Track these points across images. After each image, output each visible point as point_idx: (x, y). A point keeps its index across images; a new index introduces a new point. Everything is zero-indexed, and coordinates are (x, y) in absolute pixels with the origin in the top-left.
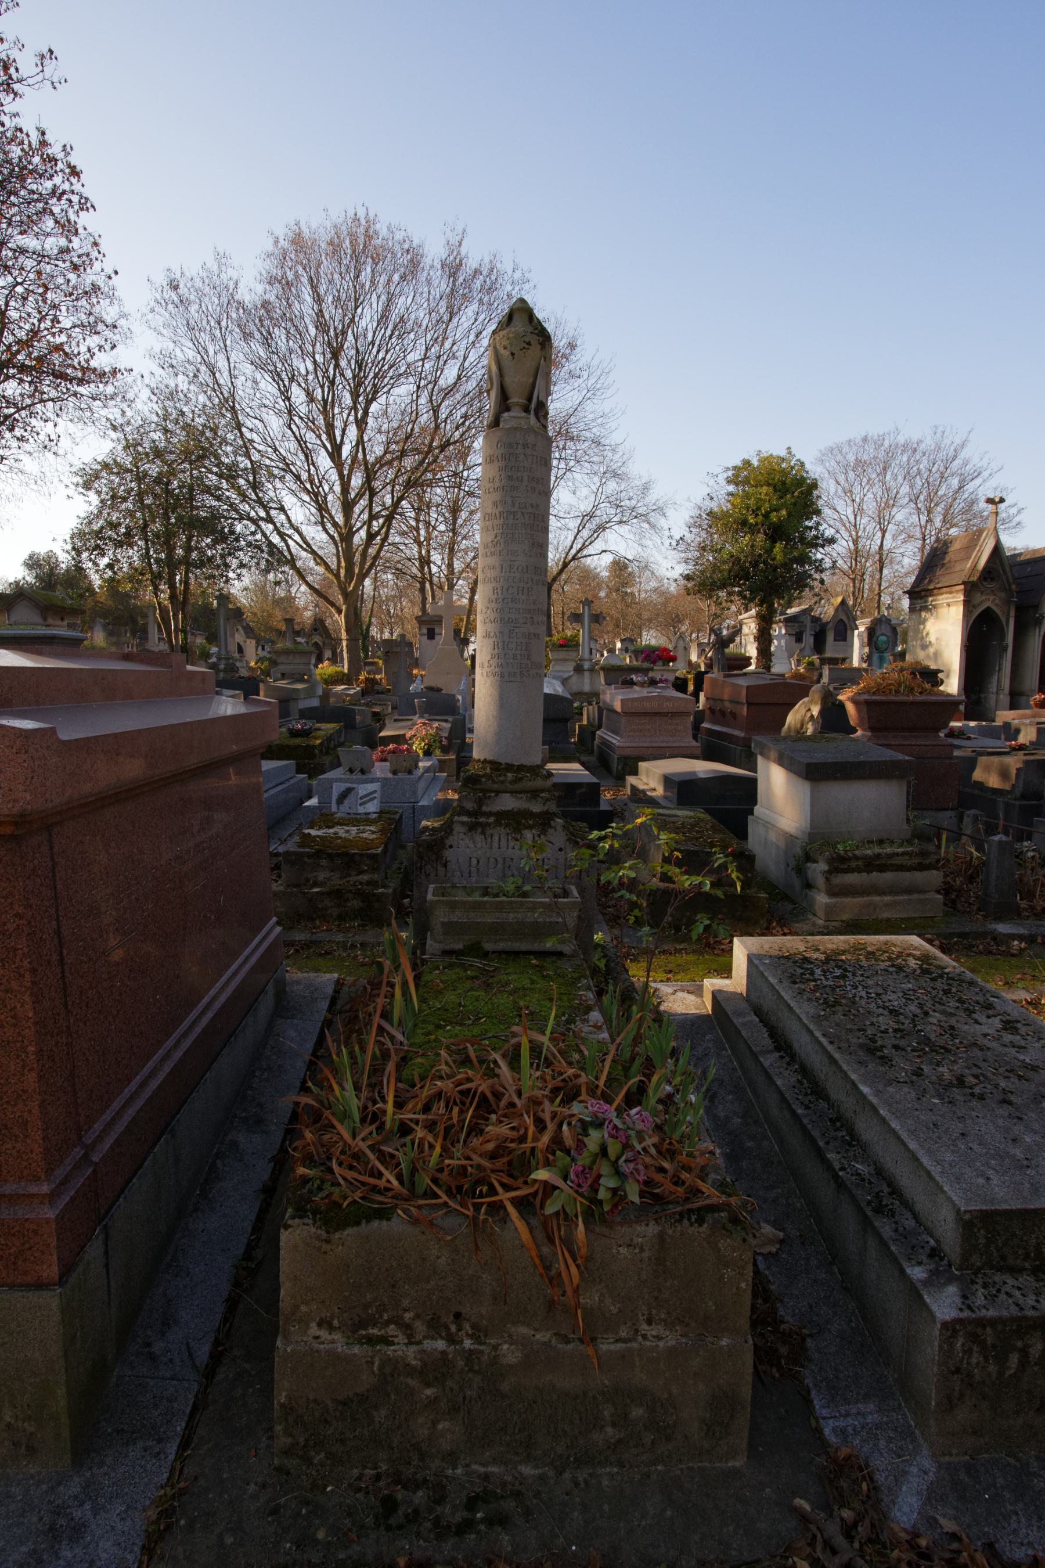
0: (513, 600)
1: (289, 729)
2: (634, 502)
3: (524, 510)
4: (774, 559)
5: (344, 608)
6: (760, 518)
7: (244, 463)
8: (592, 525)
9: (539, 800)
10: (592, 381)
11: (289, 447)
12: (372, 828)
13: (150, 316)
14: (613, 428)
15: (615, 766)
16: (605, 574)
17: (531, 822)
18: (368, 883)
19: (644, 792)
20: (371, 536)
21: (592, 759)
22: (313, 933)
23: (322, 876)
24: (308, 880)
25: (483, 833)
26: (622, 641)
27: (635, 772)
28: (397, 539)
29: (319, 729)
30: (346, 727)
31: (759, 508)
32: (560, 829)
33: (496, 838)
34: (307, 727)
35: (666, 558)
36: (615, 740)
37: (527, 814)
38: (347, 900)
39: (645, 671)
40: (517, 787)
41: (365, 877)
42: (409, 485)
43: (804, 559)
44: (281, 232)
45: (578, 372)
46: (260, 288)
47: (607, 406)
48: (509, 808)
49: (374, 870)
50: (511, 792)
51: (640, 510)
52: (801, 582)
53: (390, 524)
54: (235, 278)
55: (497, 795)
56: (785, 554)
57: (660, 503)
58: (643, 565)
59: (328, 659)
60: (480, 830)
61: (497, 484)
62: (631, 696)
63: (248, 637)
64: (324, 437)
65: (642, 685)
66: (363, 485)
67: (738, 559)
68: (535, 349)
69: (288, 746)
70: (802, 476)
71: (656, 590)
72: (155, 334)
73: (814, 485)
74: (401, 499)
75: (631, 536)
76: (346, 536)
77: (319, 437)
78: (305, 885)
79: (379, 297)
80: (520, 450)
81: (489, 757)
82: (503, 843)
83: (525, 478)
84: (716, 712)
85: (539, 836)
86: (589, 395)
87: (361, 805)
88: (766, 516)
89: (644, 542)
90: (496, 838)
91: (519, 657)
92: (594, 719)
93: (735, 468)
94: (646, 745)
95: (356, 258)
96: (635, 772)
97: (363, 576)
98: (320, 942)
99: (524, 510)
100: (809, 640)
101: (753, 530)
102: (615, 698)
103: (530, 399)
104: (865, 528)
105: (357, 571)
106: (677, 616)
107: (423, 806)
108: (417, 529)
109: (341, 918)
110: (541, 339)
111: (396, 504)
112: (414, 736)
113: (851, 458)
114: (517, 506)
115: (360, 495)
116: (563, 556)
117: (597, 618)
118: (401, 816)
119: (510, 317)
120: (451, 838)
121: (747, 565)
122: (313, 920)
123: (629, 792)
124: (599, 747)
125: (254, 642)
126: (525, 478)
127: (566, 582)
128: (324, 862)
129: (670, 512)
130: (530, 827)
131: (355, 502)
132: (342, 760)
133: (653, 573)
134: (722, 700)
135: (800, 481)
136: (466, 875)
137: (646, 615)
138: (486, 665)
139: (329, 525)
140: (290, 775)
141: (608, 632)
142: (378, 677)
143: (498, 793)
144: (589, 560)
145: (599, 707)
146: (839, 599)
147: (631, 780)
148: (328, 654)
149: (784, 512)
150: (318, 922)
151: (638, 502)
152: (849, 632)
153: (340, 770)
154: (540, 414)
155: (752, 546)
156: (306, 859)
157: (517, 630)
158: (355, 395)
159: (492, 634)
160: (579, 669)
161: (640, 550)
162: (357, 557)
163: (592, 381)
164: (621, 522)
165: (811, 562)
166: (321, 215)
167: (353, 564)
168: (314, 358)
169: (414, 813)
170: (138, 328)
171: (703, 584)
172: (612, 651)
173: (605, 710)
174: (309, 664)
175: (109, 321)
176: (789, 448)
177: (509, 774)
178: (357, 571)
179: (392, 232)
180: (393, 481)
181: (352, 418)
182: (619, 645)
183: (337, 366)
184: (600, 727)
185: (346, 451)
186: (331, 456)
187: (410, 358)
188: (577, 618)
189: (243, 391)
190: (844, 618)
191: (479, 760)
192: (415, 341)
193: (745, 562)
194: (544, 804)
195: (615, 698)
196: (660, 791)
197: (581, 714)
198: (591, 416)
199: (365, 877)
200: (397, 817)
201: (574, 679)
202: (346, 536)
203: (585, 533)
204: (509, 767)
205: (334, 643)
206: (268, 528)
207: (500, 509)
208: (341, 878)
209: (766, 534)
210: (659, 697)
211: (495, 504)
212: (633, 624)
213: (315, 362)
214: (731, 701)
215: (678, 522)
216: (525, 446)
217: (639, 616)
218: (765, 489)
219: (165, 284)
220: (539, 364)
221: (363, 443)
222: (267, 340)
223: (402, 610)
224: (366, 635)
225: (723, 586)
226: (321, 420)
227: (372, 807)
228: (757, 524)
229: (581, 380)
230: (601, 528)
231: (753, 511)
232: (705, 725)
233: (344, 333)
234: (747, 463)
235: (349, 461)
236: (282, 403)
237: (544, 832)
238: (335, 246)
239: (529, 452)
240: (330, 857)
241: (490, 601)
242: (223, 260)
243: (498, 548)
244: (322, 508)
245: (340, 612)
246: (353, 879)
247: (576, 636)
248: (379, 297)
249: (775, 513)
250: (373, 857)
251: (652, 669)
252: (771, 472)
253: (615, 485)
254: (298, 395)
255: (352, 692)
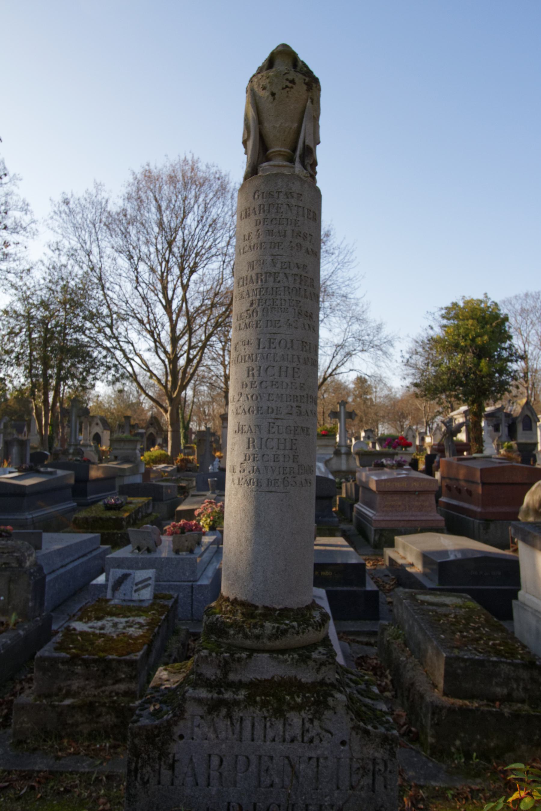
0: (273, 384)
1: (105, 504)
2: (371, 337)
3: (287, 271)
4: (481, 371)
5: (169, 409)
6: (469, 342)
7: (105, 311)
8: (342, 352)
9: (311, 663)
10: (341, 257)
11: (136, 302)
12: (141, 620)
13: (50, 221)
14: (356, 287)
15: (373, 537)
16: (352, 386)
17: (299, 700)
18: (126, 694)
19: (403, 566)
20: (189, 361)
21: (351, 527)
22: (58, 758)
23: (75, 684)
24: (60, 689)
25: (229, 716)
26: (365, 431)
27: (392, 545)
28: (210, 363)
29: (131, 503)
30: (154, 500)
31: (467, 335)
32: (341, 710)
33: (248, 724)
34: (119, 502)
35: (394, 374)
36: (368, 512)
37: (294, 686)
38: (99, 715)
39: (391, 456)
40: (278, 644)
41: (122, 687)
42: (217, 325)
43: (503, 371)
44: (139, 171)
45: (332, 251)
46: (120, 203)
47: (351, 274)
48: (268, 676)
49: (132, 678)
50: (271, 651)
51: (376, 343)
52: (503, 387)
53: (203, 353)
54: (106, 197)
55: (249, 657)
56: (489, 367)
57: (389, 338)
58: (378, 379)
59: (159, 445)
60: (224, 711)
61: (254, 241)
62: (384, 477)
63: (105, 429)
64: (161, 296)
65: (391, 467)
66: (185, 327)
67: (454, 371)
68: (300, 89)
69: (101, 519)
70: (496, 313)
71: (386, 397)
72: (52, 232)
73: (506, 319)
74: (210, 335)
75: (370, 360)
76: (174, 360)
77: (157, 295)
78: (57, 695)
79: (199, 207)
80: (282, 199)
81: (241, 597)
82: (259, 732)
83: (289, 233)
84: (452, 487)
85: (311, 721)
86: (339, 267)
87: (136, 591)
88: (473, 340)
89: (379, 363)
90: (248, 724)
91: (281, 459)
92: (351, 493)
93: (446, 308)
94: (398, 518)
95: (185, 185)
96: (392, 545)
97: (184, 387)
98: (61, 773)
99: (287, 271)
100: (504, 429)
101: (464, 350)
102: (372, 478)
103: (294, 150)
104: (532, 353)
105: (179, 383)
106: (402, 413)
107: (201, 585)
108: (223, 356)
109: (92, 736)
110: (307, 79)
111: (208, 338)
112: (201, 513)
113: (518, 307)
114: (279, 265)
115: (183, 334)
116: (323, 374)
117: (350, 415)
118: (176, 602)
119: (271, 62)
120: (181, 723)
121: (461, 375)
122: (61, 738)
123: (387, 563)
124: (357, 518)
125: (109, 432)
126: (289, 233)
127: (325, 392)
128: (79, 669)
129: (396, 344)
130: (298, 708)
131: (179, 338)
132: (131, 539)
133: (385, 385)
134: (458, 480)
135: (495, 316)
136: (202, 780)
137: (381, 413)
138: (238, 469)
139: (160, 352)
140: (95, 546)
141: (354, 426)
142: (191, 457)
143: (252, 651)
144: (341, 376)
145: (356, 485)
146: (524, 401)
147: (389, 552)
148: (159, 441)
149: (486, 337)
150: (65, 742)
151: (374, 336)
152: (533, 424)
153: (129, 548)
154: (307, 161)
155: (464, 362)
156: (60, 666)
157: (279, 423)
158: (182, 269)
159: (246, 428)
160: (337, 453)
161: (376, 369)
162: (180, 376)
163: (341, 257)
164: (362, 351)
165: (509, 374)
166: (163, 158)
167: (177, 377)
168: (156, 246)
169: (192, 591)
170: (41, 228)
171: (430, 388)
172: (358, 438)
173: (362, 487)
174: (135, 449)
175: (24, 225)
176: (486, 294)
177: (268, 624)
178: (179, 383)
179: (209, 168)
180: (206, 323)
181: (179, 284)
182: (363, 434)
183: (170, 251)
184: (357, 500)
185: (175, 305)
186: (165, 307)
187: (219, 246)
188: (335, 415)
189: (107, 264)
190: (529, 414)
191: (227, 599)
192: (223, 235)
193: (459, 373)
194: (318, 670)
195: (372, 478)
196: (418, 568)
197: (340, 488)
198: (341, 280)
199: (122, 687)
200: (170, 603)
201: (334, 461)
202: (174, 360)
203: (338, 357)
204: (268, 613)
205: (162, 432)
206: (118, 354)
207: (257, 270)
208: (96, 688)
209: (474, 353)
210: (408, 479)
211: (251, 265)
212: (373, 420)
213: (157, 249)
214: (467, 481)
215: (402, 348)
216: (289, 195)
217: (376, 414)
218: (470, 322)
219: (60, 201)
220: (305, 107)
221: (186, 299)
222: (125, 235)
223: (213, 411)
224: (187, 428)
225: (444, 390)
226: (159, 287)
227: (147, 594)
228: (466, 346)
229: (333, 256)
230: (349, 354)
231: (463, 337)
232: (443, 499)
233: (176, 231)
234: (455, 305)
235: (177, 311)
236: (132, 273)
237: (317, 715)
238: (172, 179)
239: (293, 202)
240: (86, 663)
241: (244, 385)
242: (100, 187)
243: (255, 318)
244: (157, 341)
245: (166, 411)
246: (109, 688)
247: (334, 428)
248: (199, 207)
249: (479, 338)
250: (131, 664)
251: (397, 454)
252: (473, 310)
253: (358, 326)
254: (142, 267)
255: (169, 469)
